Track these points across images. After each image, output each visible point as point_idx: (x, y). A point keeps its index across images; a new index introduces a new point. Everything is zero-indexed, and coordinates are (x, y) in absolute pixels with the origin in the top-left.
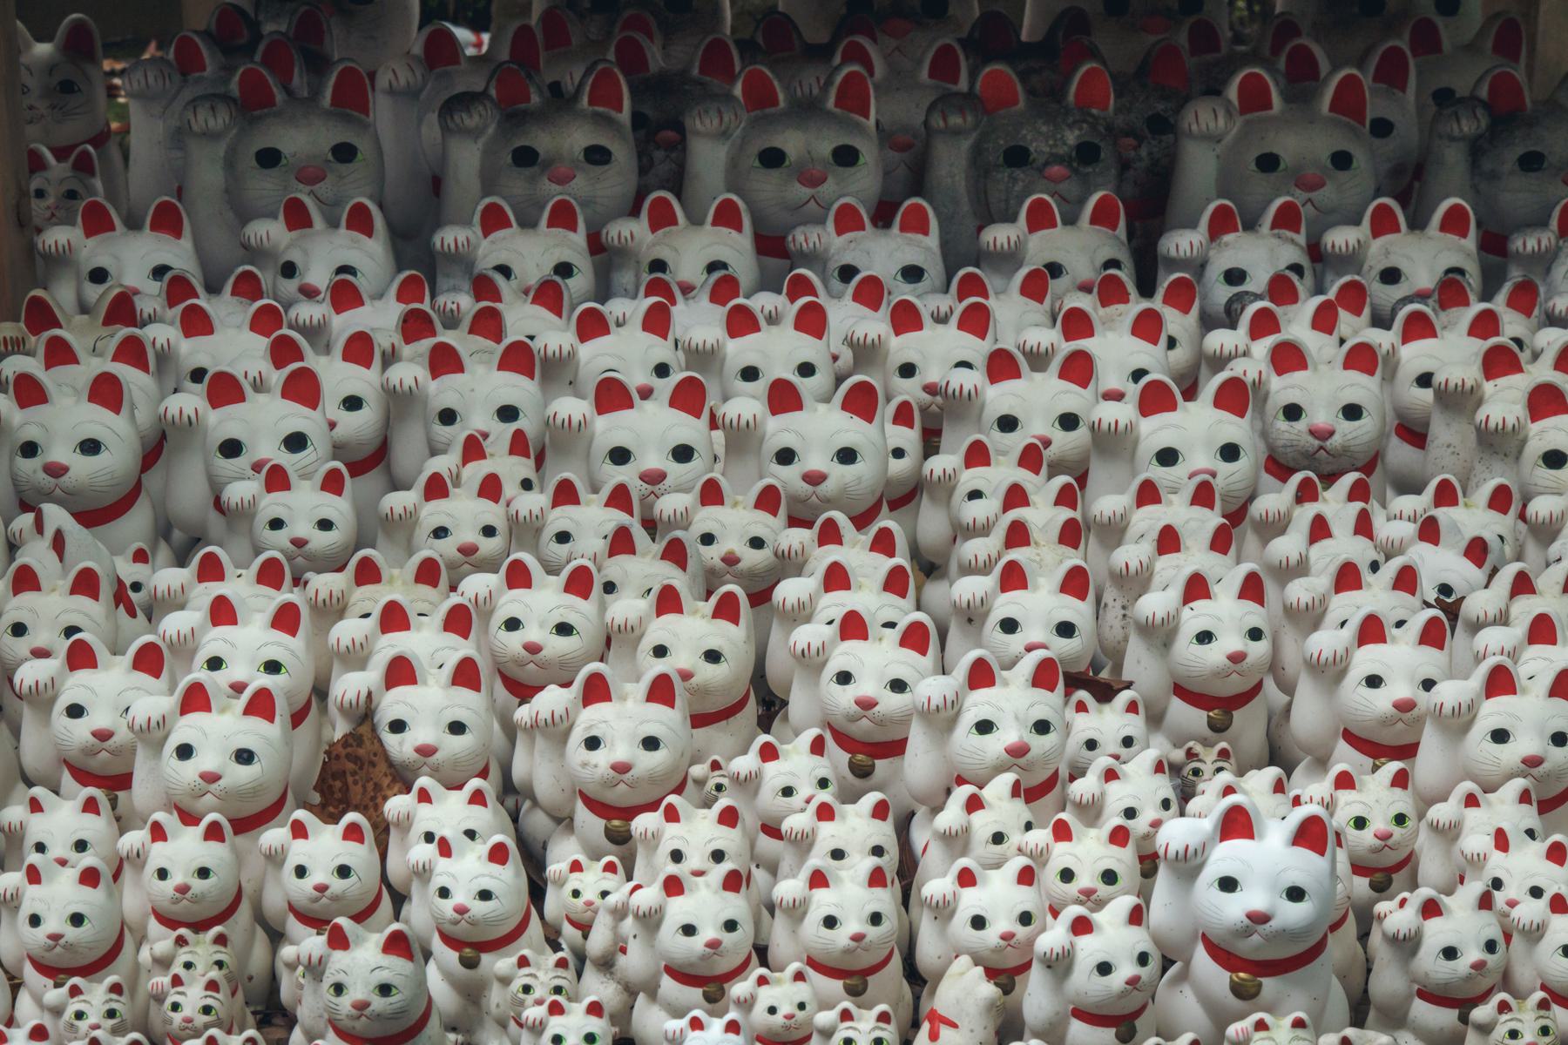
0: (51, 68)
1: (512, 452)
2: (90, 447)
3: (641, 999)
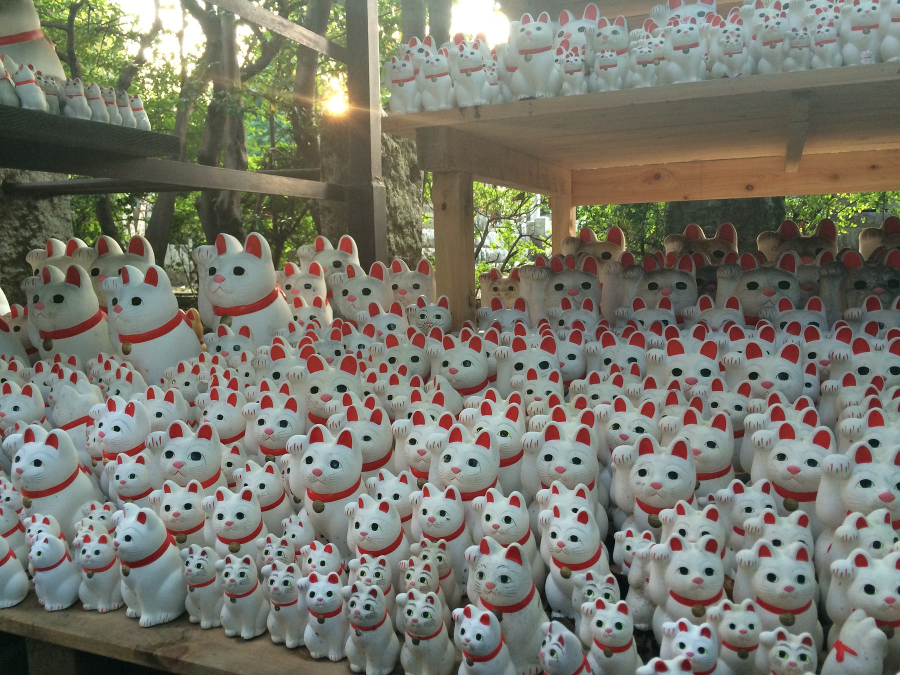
0: (506, 282)
1: (632, 373)
2: (466, 363)
3: (658, 609)
